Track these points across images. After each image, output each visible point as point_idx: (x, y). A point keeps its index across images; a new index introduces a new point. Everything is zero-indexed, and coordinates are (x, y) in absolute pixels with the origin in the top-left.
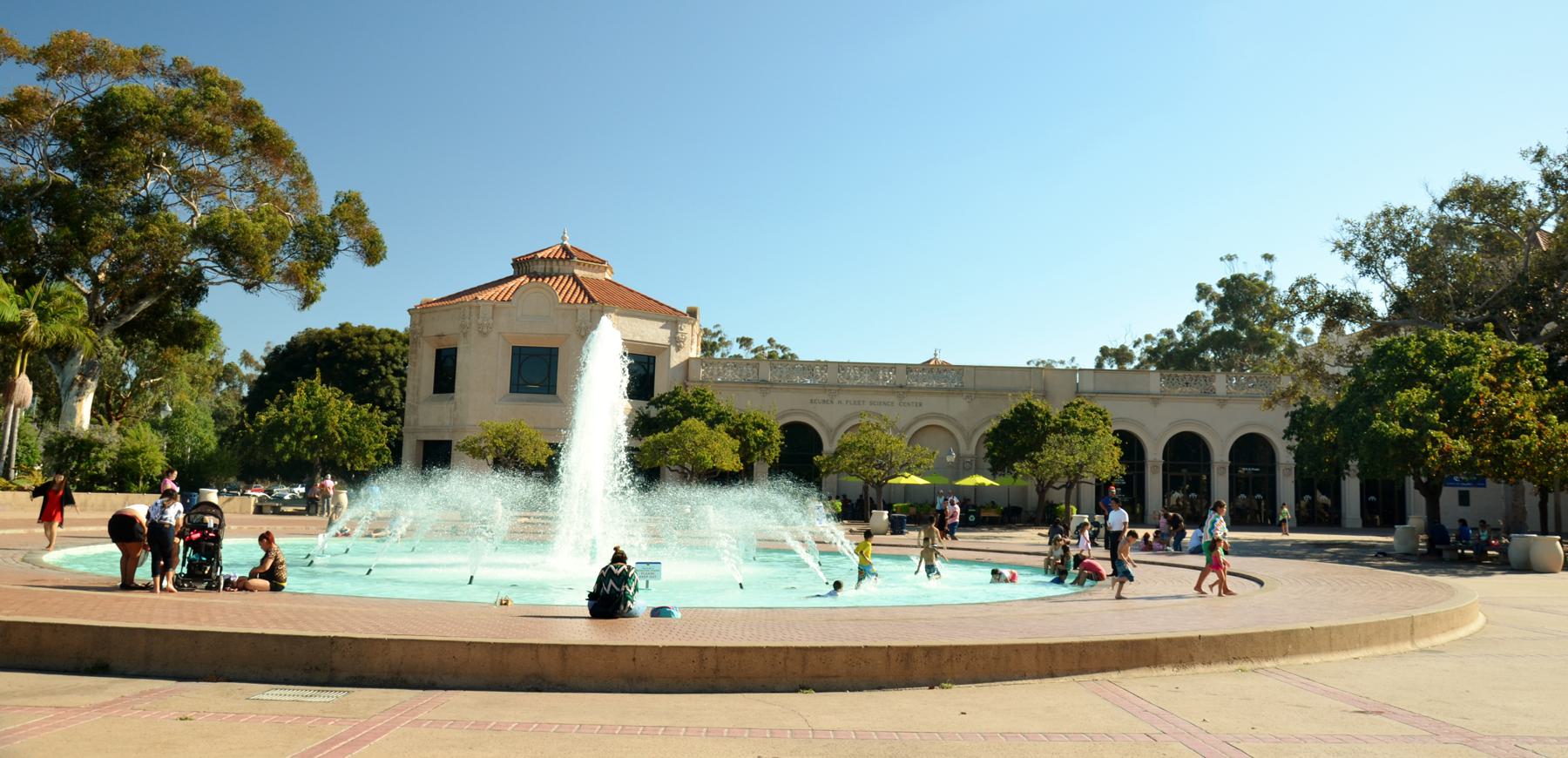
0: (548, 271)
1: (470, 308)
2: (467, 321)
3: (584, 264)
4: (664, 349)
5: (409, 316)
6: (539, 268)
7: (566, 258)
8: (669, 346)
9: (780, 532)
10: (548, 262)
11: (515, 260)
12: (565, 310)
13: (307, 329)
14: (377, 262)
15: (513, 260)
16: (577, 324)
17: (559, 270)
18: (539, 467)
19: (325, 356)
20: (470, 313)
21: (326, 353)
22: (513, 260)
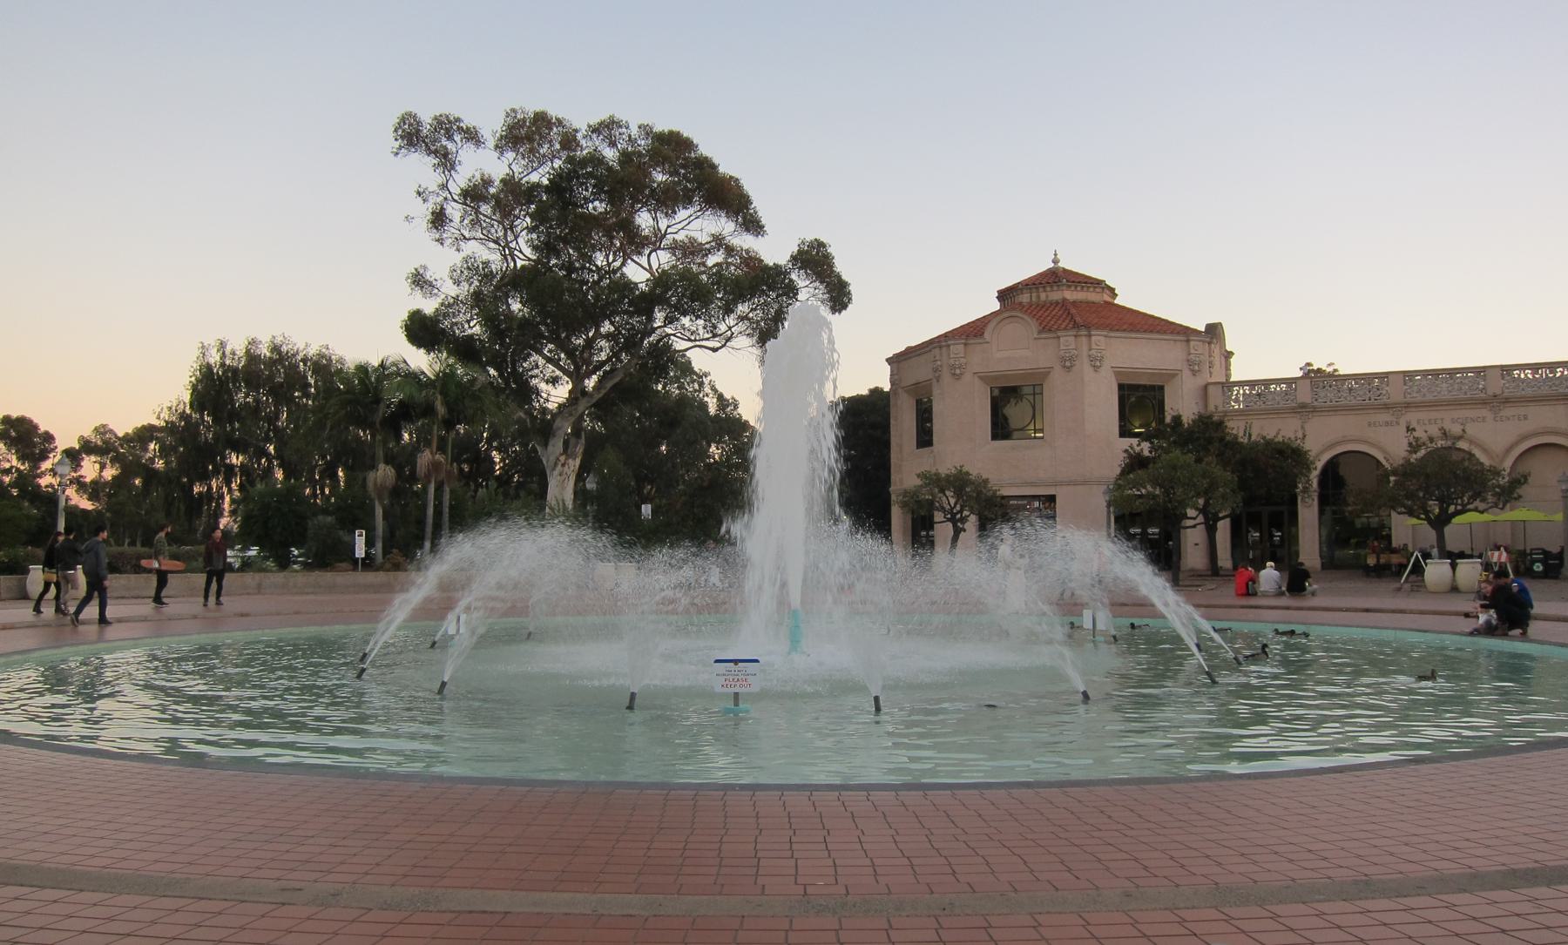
5: (889, 367)
18: (1051, 517)
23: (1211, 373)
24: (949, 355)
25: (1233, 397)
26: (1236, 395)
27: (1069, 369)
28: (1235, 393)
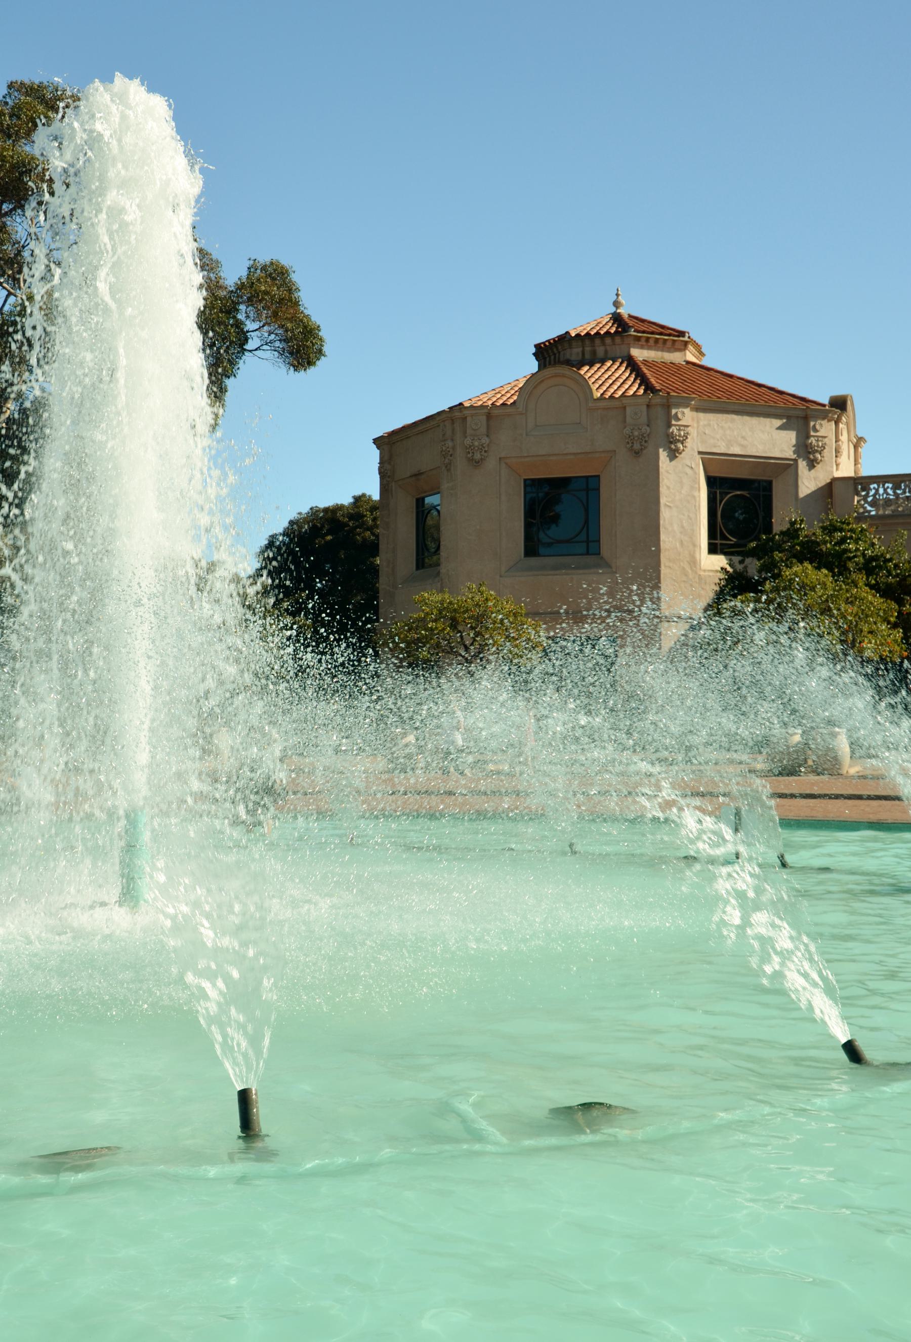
0: (587, 356)
1: (453, 421)
2: (450, 444)
3: (648, 339)
4: (787, 468)
6: (575, 353)
7: (616, 332)
8: (795, 460)
9: (9, 590)
10: (587, 342)
11: (537, 346)
12: (605, 409)
13: (311, 509)
14: (310, 363)
15: (536, 346)
16: (627, 431)
17: (606, 352)
19: (327, 542)
20: (453, 430)
21: (329, 538)
22: (536, 346)
23: (837, 465)
24: (465, 432)
25: (870, 499)
26: (874, 496)
27: (637, 453)
28: (872, 492)
